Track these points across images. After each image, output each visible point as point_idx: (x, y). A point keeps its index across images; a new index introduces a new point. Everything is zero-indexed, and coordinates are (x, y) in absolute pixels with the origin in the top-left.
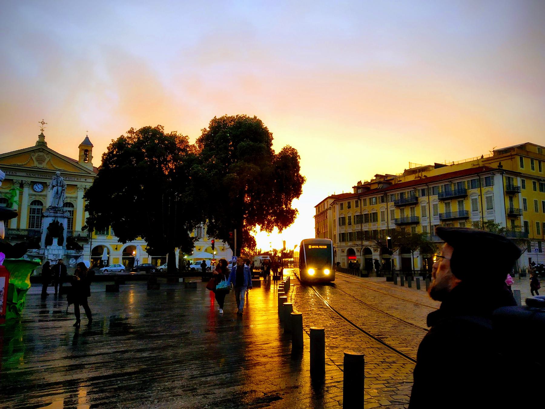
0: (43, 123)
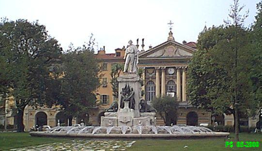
0: (92, 35)
